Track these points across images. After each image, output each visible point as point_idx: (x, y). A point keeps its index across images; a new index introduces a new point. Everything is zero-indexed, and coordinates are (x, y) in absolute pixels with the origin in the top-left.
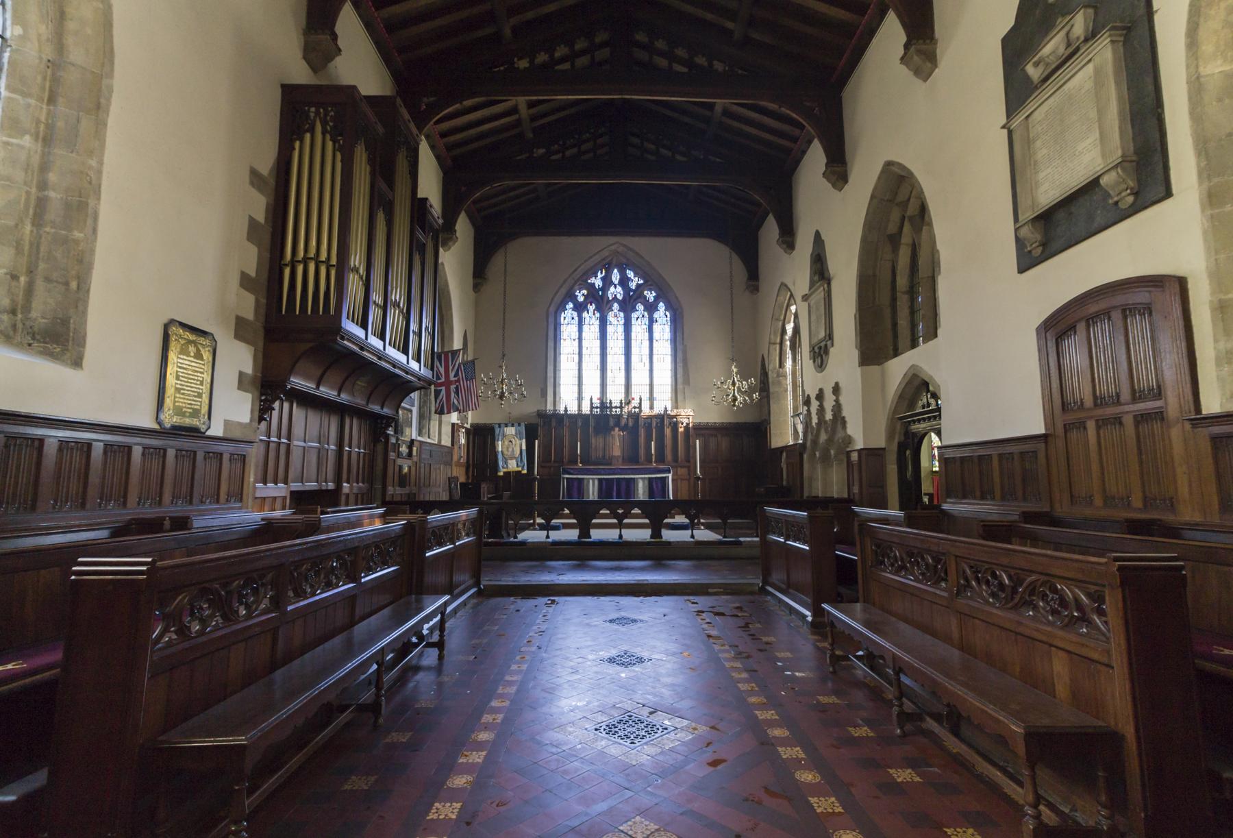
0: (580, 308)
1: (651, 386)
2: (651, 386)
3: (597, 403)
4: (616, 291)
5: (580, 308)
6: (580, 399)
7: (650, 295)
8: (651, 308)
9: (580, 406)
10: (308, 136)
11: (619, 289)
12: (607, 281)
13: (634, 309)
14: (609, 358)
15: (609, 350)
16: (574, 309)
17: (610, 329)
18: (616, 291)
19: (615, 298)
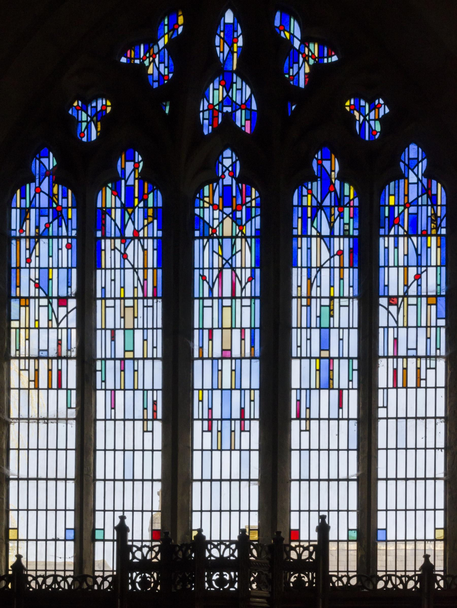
0: (84, 173)
1: (435, 550)
2: (435, 550)
3: (141, 530)
4: (229, 98)
5: (84, 173)
6: (83, 535)
7: (371, 117)
8: (372, 169)
9: (84, 556)
10: (429, 214)
11: (242, 92)
12: (195, 63)
13: (302, 175)
14: (202, 375)
15: (296, 465)
16: (56, 176)
17: (205, 255)
18: (229, 98)
19: (226, 132)
